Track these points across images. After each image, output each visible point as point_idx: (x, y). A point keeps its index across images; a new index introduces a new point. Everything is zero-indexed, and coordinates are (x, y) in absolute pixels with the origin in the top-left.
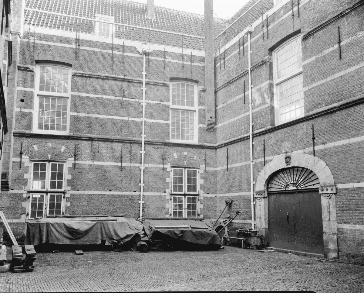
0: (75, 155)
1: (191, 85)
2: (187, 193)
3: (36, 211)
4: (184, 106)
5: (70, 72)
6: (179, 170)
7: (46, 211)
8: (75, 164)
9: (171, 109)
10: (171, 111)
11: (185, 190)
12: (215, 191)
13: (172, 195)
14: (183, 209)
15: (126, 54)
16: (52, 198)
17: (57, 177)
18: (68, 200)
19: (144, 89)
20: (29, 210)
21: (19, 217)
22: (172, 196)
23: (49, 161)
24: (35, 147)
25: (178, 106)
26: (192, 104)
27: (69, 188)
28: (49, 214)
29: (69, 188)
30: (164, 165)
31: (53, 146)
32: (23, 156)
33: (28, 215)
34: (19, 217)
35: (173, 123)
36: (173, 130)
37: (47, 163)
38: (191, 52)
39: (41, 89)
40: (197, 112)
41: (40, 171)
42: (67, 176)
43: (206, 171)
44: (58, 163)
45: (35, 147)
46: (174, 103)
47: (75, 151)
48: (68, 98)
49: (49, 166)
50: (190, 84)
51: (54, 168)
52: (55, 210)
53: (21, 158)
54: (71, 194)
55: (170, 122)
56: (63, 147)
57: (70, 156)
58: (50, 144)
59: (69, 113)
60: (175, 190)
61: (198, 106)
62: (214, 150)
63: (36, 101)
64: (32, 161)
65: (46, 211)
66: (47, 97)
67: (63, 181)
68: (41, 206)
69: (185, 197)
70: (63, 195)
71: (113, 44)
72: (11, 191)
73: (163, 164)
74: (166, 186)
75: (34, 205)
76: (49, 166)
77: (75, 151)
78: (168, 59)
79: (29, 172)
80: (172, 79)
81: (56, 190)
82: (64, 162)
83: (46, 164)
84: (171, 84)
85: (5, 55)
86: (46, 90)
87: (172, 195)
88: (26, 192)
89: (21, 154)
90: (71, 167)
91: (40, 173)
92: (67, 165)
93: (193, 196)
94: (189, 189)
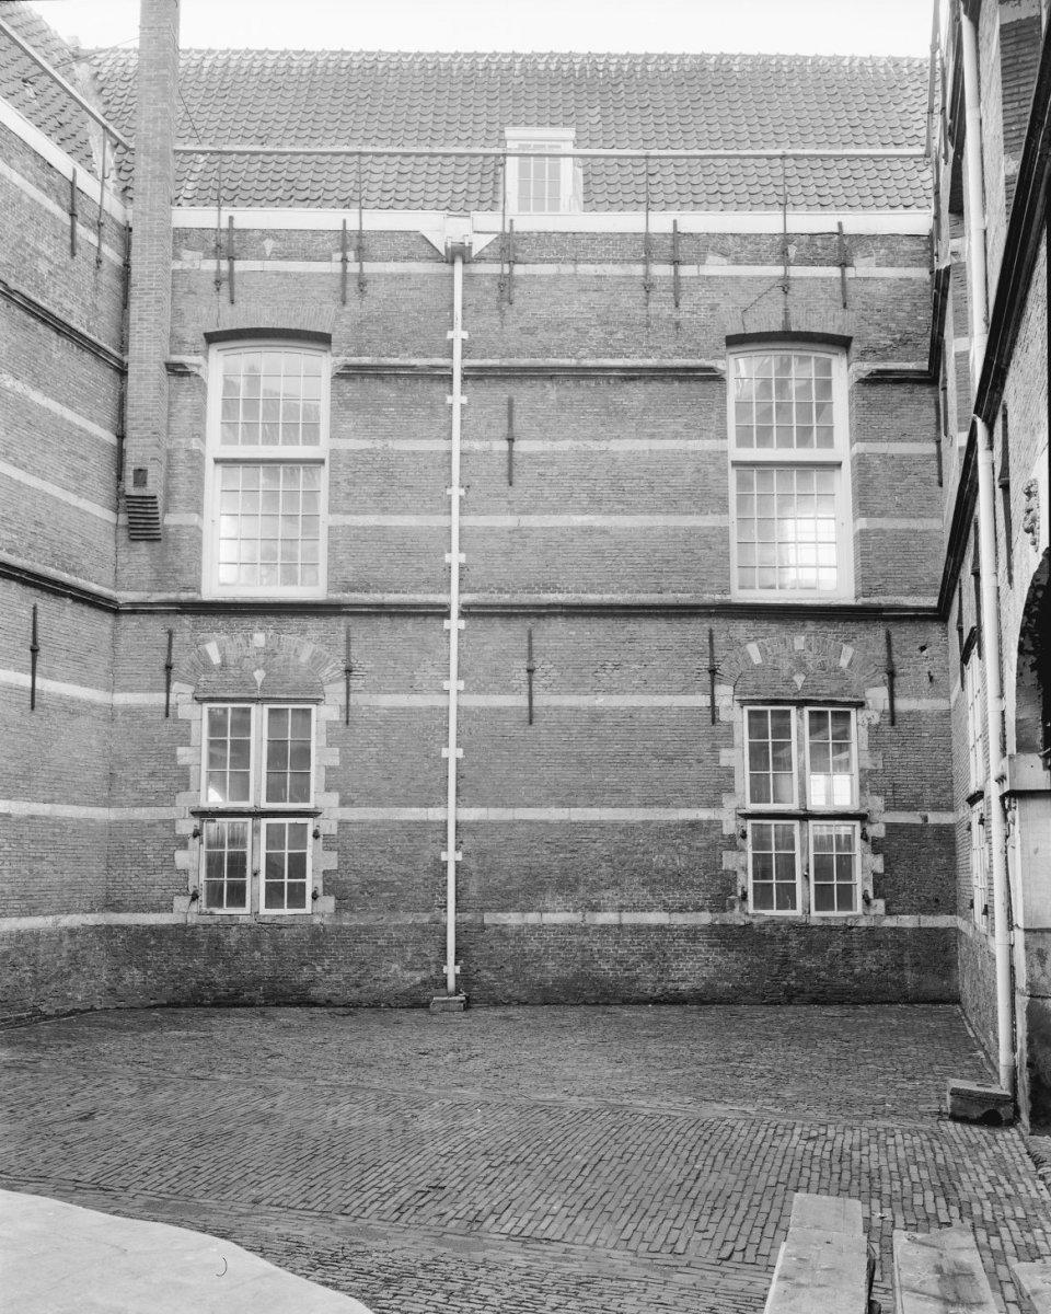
4: (271, 448)
6: (233, 709)
7: (257, 887)
9: (735, 464)
16: (275, 838)
17: (289, 759)
18: (329, 843)
19: (457, 399)
20: (200, 879)
24: (753, 650)
26: (827, 438)
27: (335, 797)
29: (335, 797)
32: (175, 686)
33: (195, 897)
37: (253, 707)
38: (344, 222)
40: (846, 468)
41: (229, 738)
42: (322, 756)
43: (893, 716)
45: (753, 650)
46: (744, 439)
48: (322, 462)
49: (259, 715)
50: (814, 355)
52: (835, 882)
54: (889, 826)
56: (305, 644)
58: (260, 636)
59: (325, 519)
61: (852, 444)
62: (109, 619)
64: (743, 703)
67: (313, 770)
68: (238, 865)
69: (801, 825)
71: (647, 234)
75: (214, 865)
76: (259, 715)
78: (862, 268)
83: (849, 713)
91: (230, 749)
92: (325, 714)
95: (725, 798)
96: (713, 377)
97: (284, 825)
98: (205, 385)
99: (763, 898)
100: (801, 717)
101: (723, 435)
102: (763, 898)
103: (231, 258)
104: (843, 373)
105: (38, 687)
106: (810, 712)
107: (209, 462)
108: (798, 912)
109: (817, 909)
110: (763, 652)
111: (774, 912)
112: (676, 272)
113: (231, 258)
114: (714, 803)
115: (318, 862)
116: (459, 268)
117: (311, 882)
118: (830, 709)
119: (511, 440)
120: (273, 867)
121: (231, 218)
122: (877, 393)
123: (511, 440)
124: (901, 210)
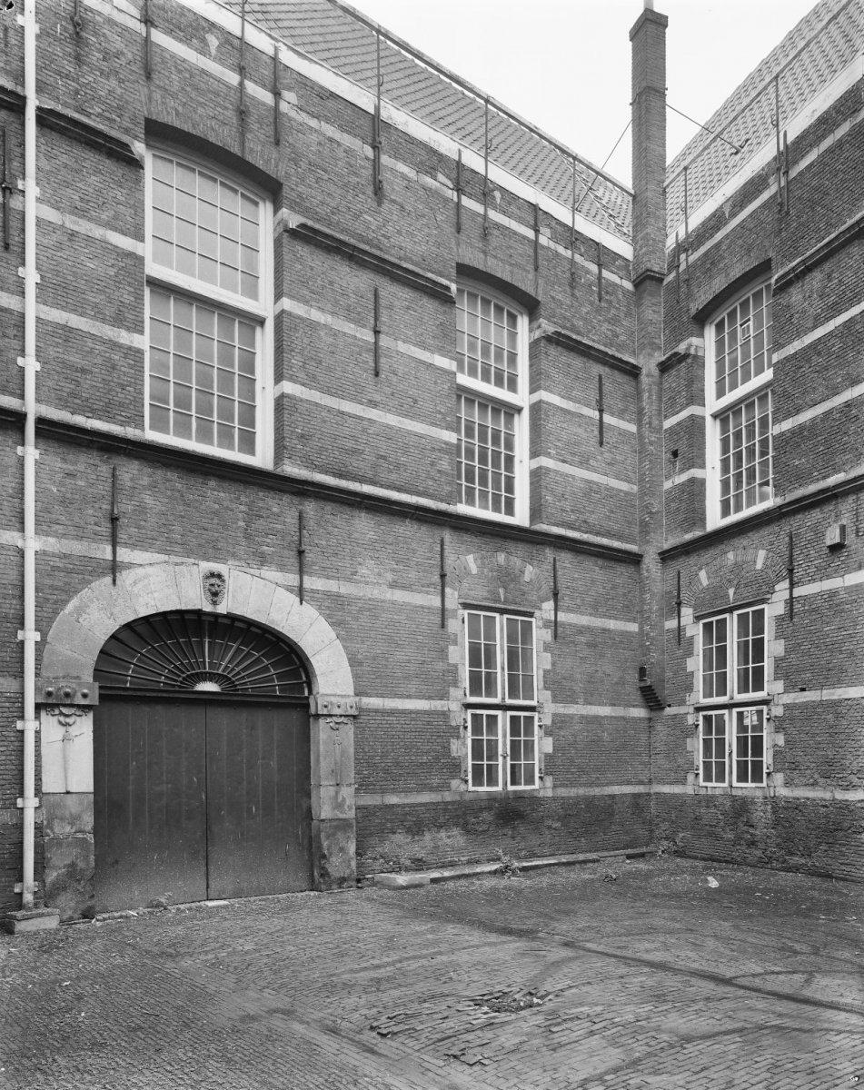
0: (791, 571)
1: (483, 299)
2: (509, 701)
8: (791, 602)
12: (831, 676)
13: (468, 706)
14: (500, 759)
21: (683, 782)
22: (470, 712)
23: (730, 610)
28: (724, 781)
31: (739, 559)
34: (683, 782)
44: (750, 610)
47: (791, 556)
49: (732, 623)
57: (779, 579)
60: (475, 690)
67: (765, 664)
70: (765, 708)
72: (668, 711)
77: (791, 556)
79: (695, 653)
82: (763, 601)
85: (38, 662)
88: (691, 710)
89: (679, 604)
90: (782, 612)
105: (297, 577)
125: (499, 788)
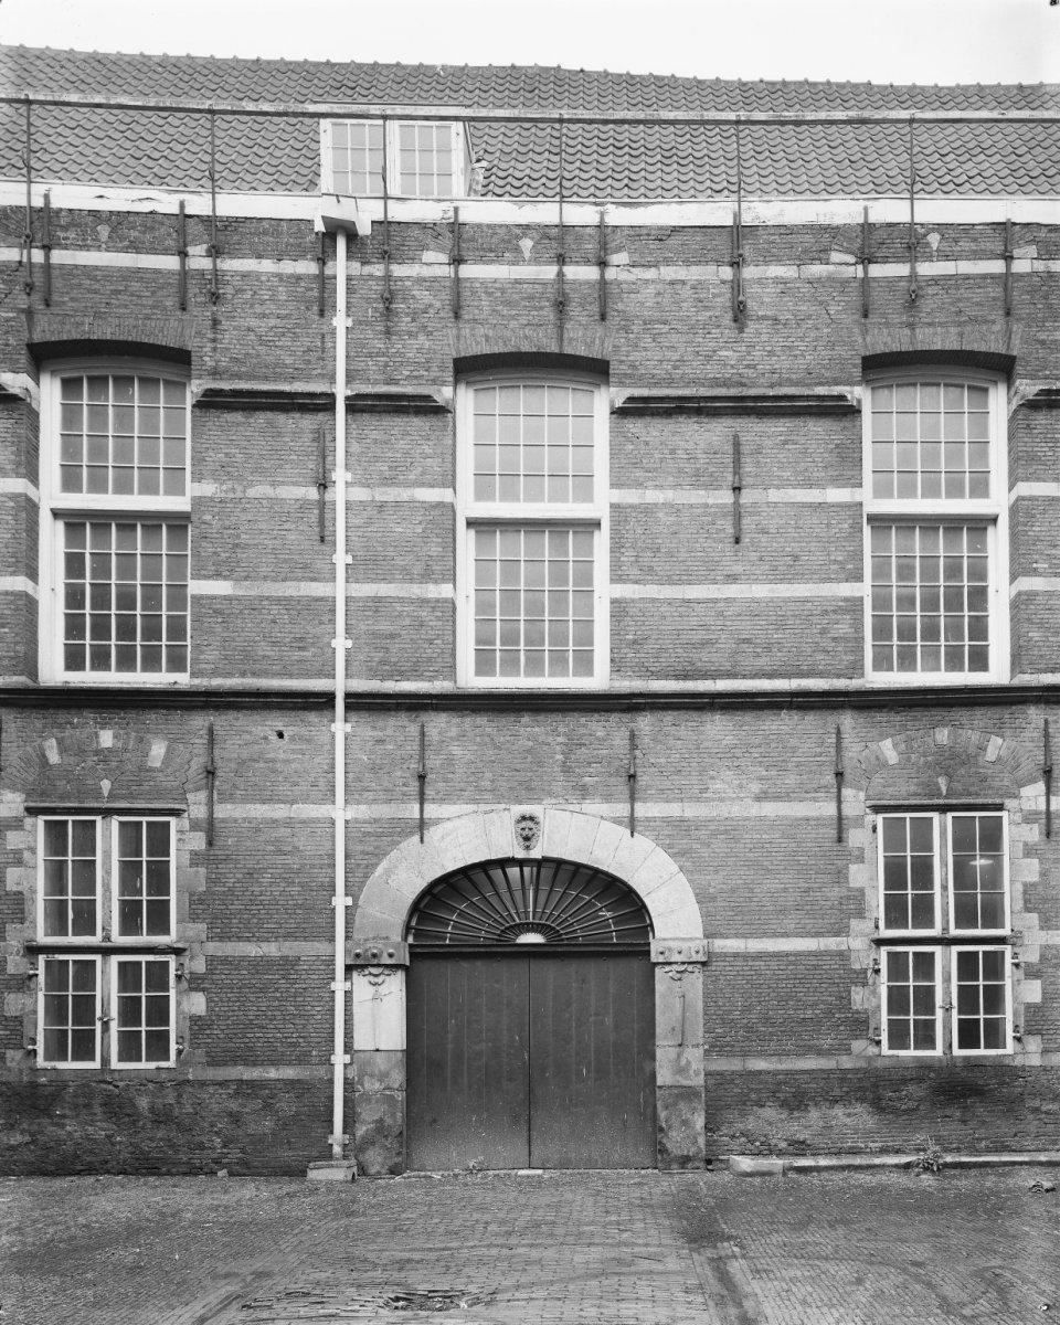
3: (978, 1020)
4: (559, 505)
5: (602, 401)
10: (466, 540)
11: (943, 916)
13: (880, 942)
15: (467, 271)
22: (884, 950)
23: (107, 813)
25: (975, 501)
30: (638, 806)
32: (847, 792)
35: (881, 602)
36: (881, 630)
39: (70, 481)
49: (109, 834)
51: (130, 834)
53: (839, 802)
55: (864, 589)
63: (52, 542)
64: (877, 809)
65: (109, 1039)
66: (101, 520)
70: (172, 960)
73: (633, 799)
74: (856, 904)
76: (109, 834)
78: (620, 268)
80: (469, 369)
81: (144, 939)
84: (466, 402)
86: (949, 495)
87: (880, 942)
93: (151, 958)
94: (130, 922)
95: (1034, 918)
96: (845, 411)
97: (139, 963)
98: (37, 415)
99: (57, 1049)
100: (107, 829)
101: (450, 481)
102: (898, 1037)
103: (47, 248)
104: (999, 404)
106: (46, 822)
107: (45, 518)
108: (938, 1052)
109: (961, 1046)
110: (63, 750)
111: (912, 1053)
112: (456, 272)
113: (47, 248)
114: (840, 930)
115: (184, 1005)
116: (341, 266)
117: (1009, 1016)
118: (70, 818)
119: (737, 489)
120: (129, 1010)
121: (47, 197)
122: (635, 426)
123: (737, 489)
124: (808, 195)
125: (96, 1065)
